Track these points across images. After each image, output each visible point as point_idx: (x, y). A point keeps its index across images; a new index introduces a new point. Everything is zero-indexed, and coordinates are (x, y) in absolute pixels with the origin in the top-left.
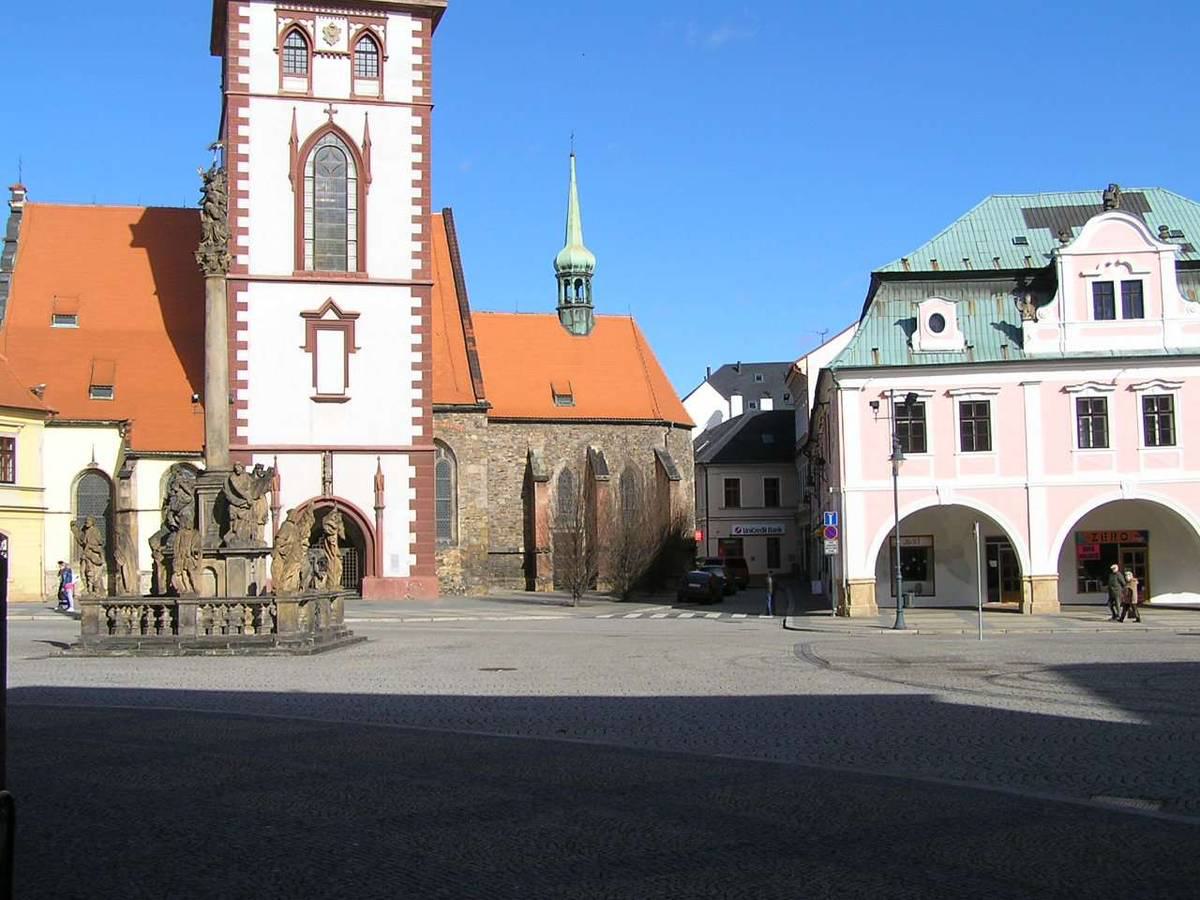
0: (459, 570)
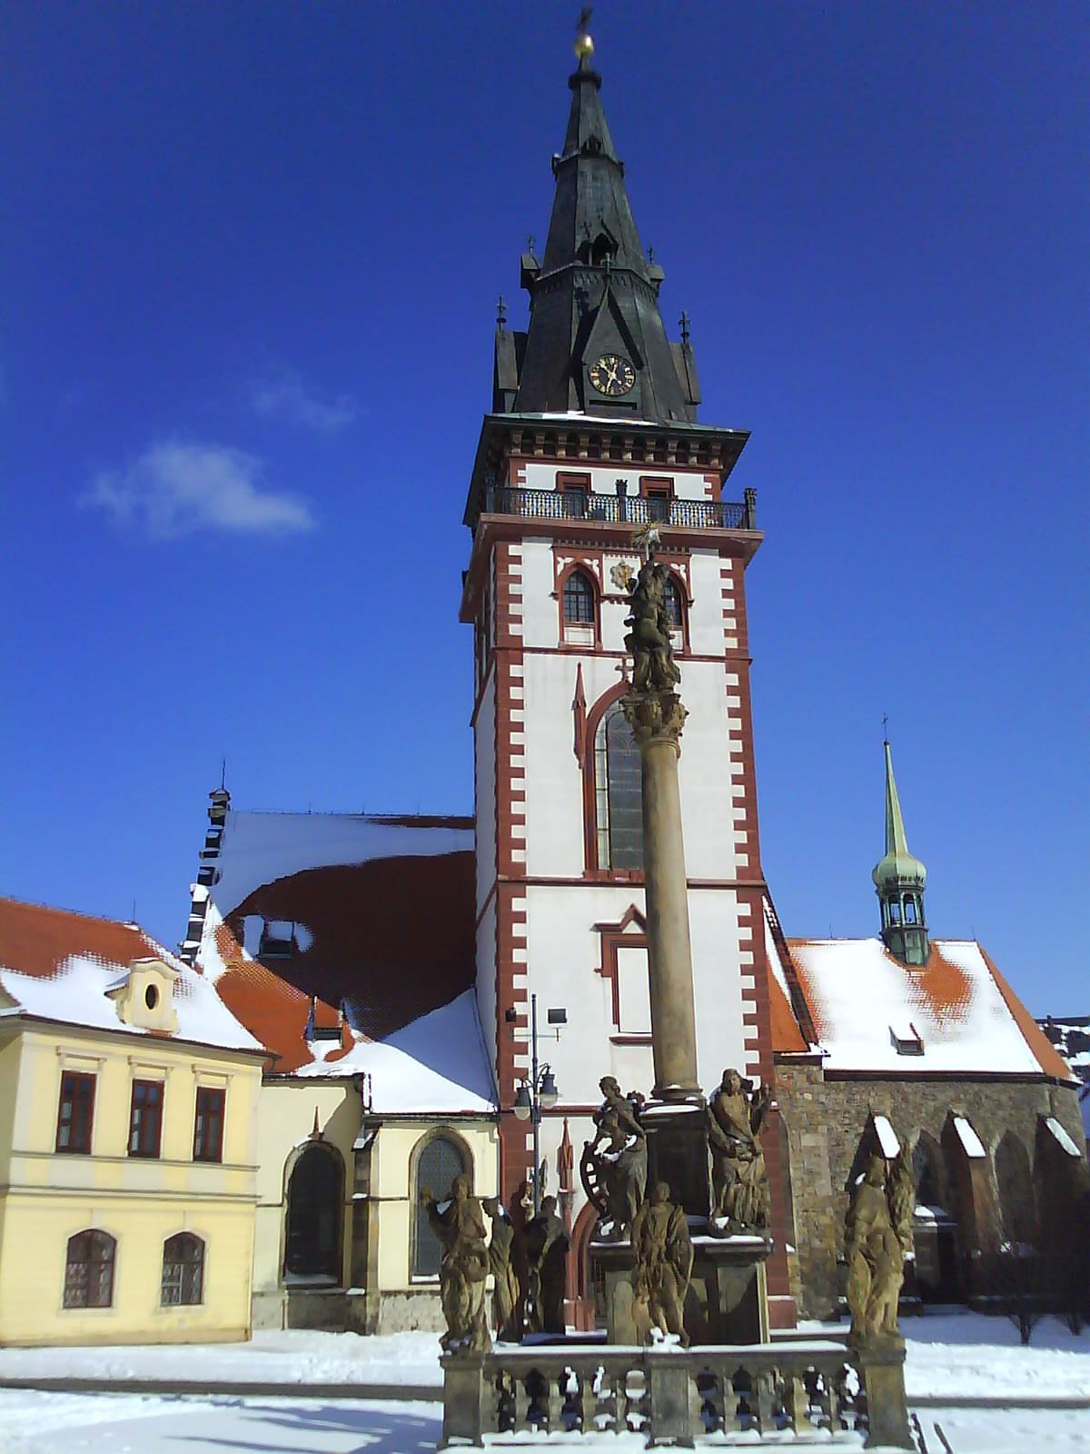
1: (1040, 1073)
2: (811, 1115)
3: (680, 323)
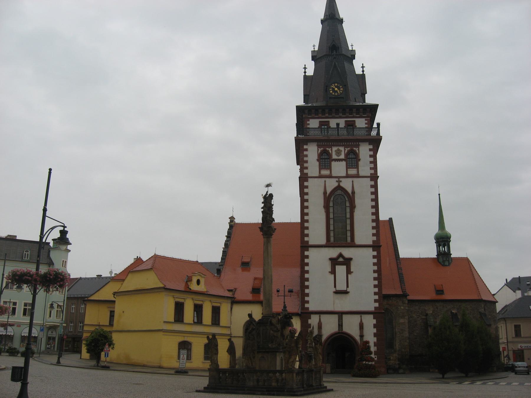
0: (397, 362)
1: (402, 294)
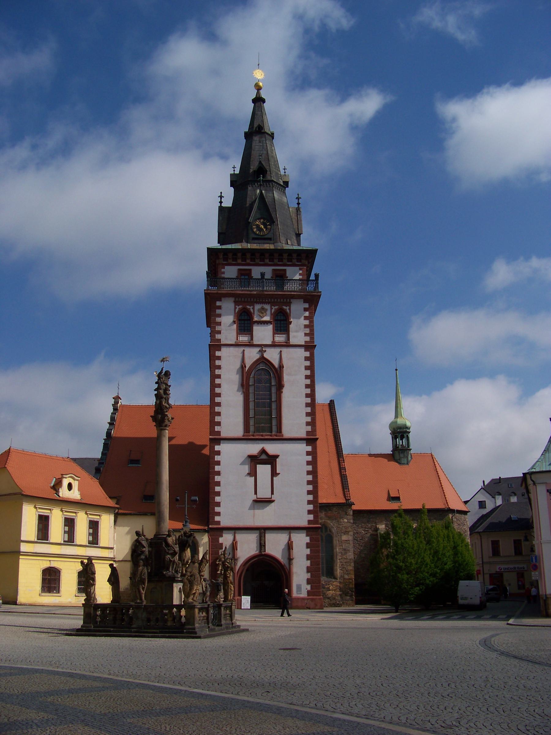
0: (338, 593)
2: (346, 528)
3: (296, 199)
